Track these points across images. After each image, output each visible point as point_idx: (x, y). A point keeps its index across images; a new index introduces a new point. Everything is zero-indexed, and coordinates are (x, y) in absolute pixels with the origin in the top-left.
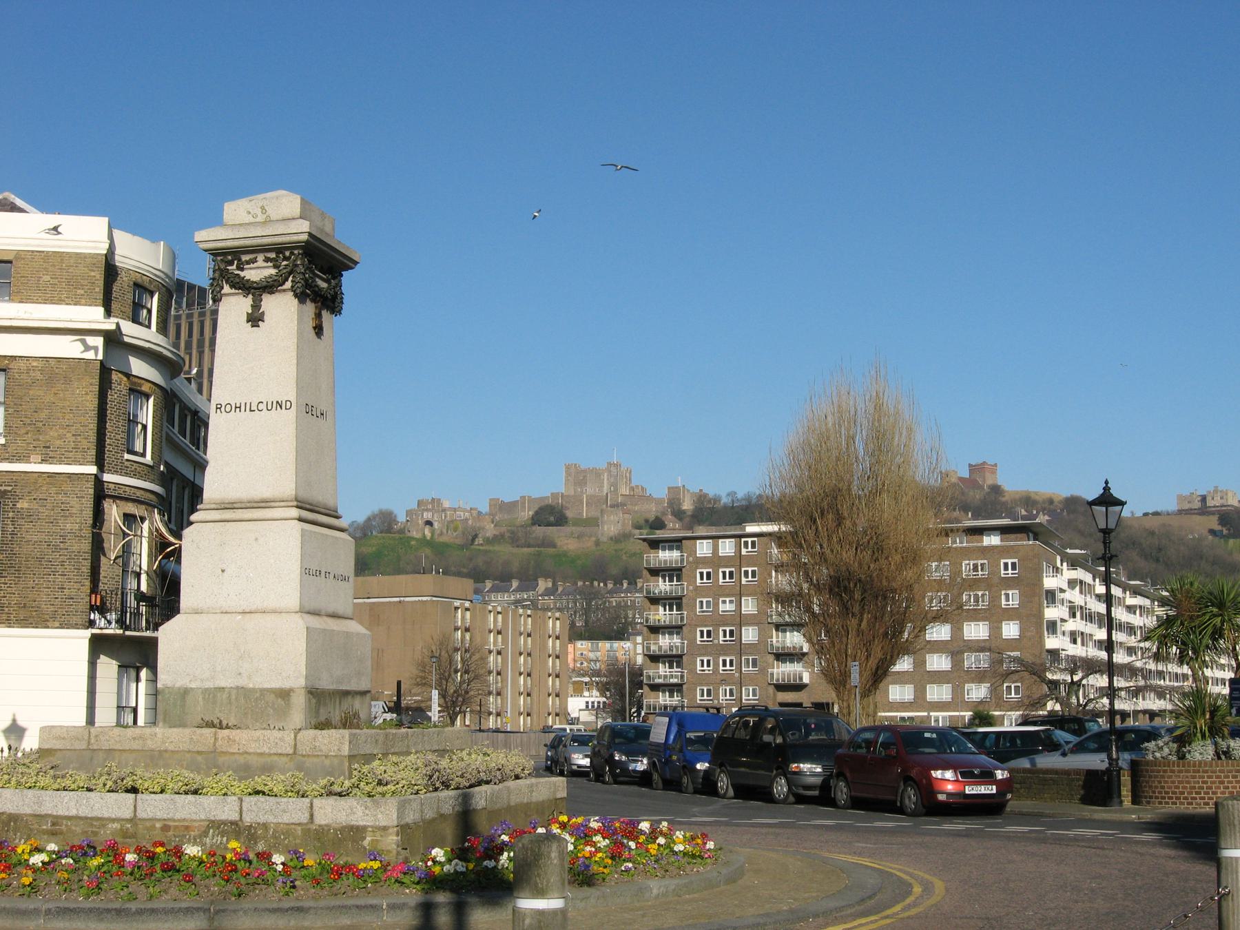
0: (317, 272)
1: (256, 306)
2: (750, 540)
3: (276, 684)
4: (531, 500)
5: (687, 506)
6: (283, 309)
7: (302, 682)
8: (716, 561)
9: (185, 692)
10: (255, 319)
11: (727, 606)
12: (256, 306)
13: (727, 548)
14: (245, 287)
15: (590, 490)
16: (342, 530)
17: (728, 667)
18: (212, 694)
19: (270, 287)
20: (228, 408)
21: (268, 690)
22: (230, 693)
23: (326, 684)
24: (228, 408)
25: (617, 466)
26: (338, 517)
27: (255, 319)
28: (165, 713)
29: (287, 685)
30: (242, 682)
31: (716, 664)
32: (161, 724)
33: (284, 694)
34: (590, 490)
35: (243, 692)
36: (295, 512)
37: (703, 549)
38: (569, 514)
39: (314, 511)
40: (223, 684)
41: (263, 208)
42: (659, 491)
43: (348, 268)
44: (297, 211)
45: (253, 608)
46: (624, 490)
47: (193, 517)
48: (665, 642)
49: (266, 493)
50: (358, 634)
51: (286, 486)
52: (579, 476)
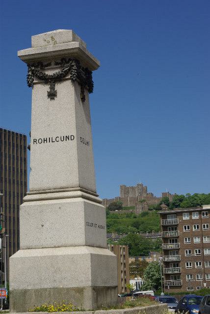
0: (79, 70)
1: (52, 88)
2: (205, 212)
3: (75, 285)
4: (107, 201)
5: (171, 200)
6: (67, 90)
7: (90, 284)
8: (192, 222)
9: (25, 292)
10: (52, 95)
11: (197, 240)
12: (52, 88)
13: (195, 217)
14: (45, 80)
15: (131, 195)
16: (99, 202)
17: (189, 266)
18: (40, 293)
19: (59, 79)
20: (40, 141)
21: (73, 289)
22: (50, 291)
23: (100, 284)
24: (40, 141)
25: (142, 185)
26: (97, 196)
27: (52, 95)
28: (14, 304)
29: (81, 285)
30: (56, 285)
31: (194, 265)
32: (12, 310)
33: (80, 291)
34: (131, 195)
35: (58, 291)
36: (79, 193)
37: (186, 218)
38: (123, 206)
39: (88, 193)
40: (46, 286)
41: (52, 38)
42: (158, 195)
43: (95, 69)
44: (71, 38)
45: (60, 245)
46: (145, 195)
47: (25, 198)
48: (172, 258)
49: (64, 185)
50: (112, 256)
51: (74, 180)
52: (125, 190)
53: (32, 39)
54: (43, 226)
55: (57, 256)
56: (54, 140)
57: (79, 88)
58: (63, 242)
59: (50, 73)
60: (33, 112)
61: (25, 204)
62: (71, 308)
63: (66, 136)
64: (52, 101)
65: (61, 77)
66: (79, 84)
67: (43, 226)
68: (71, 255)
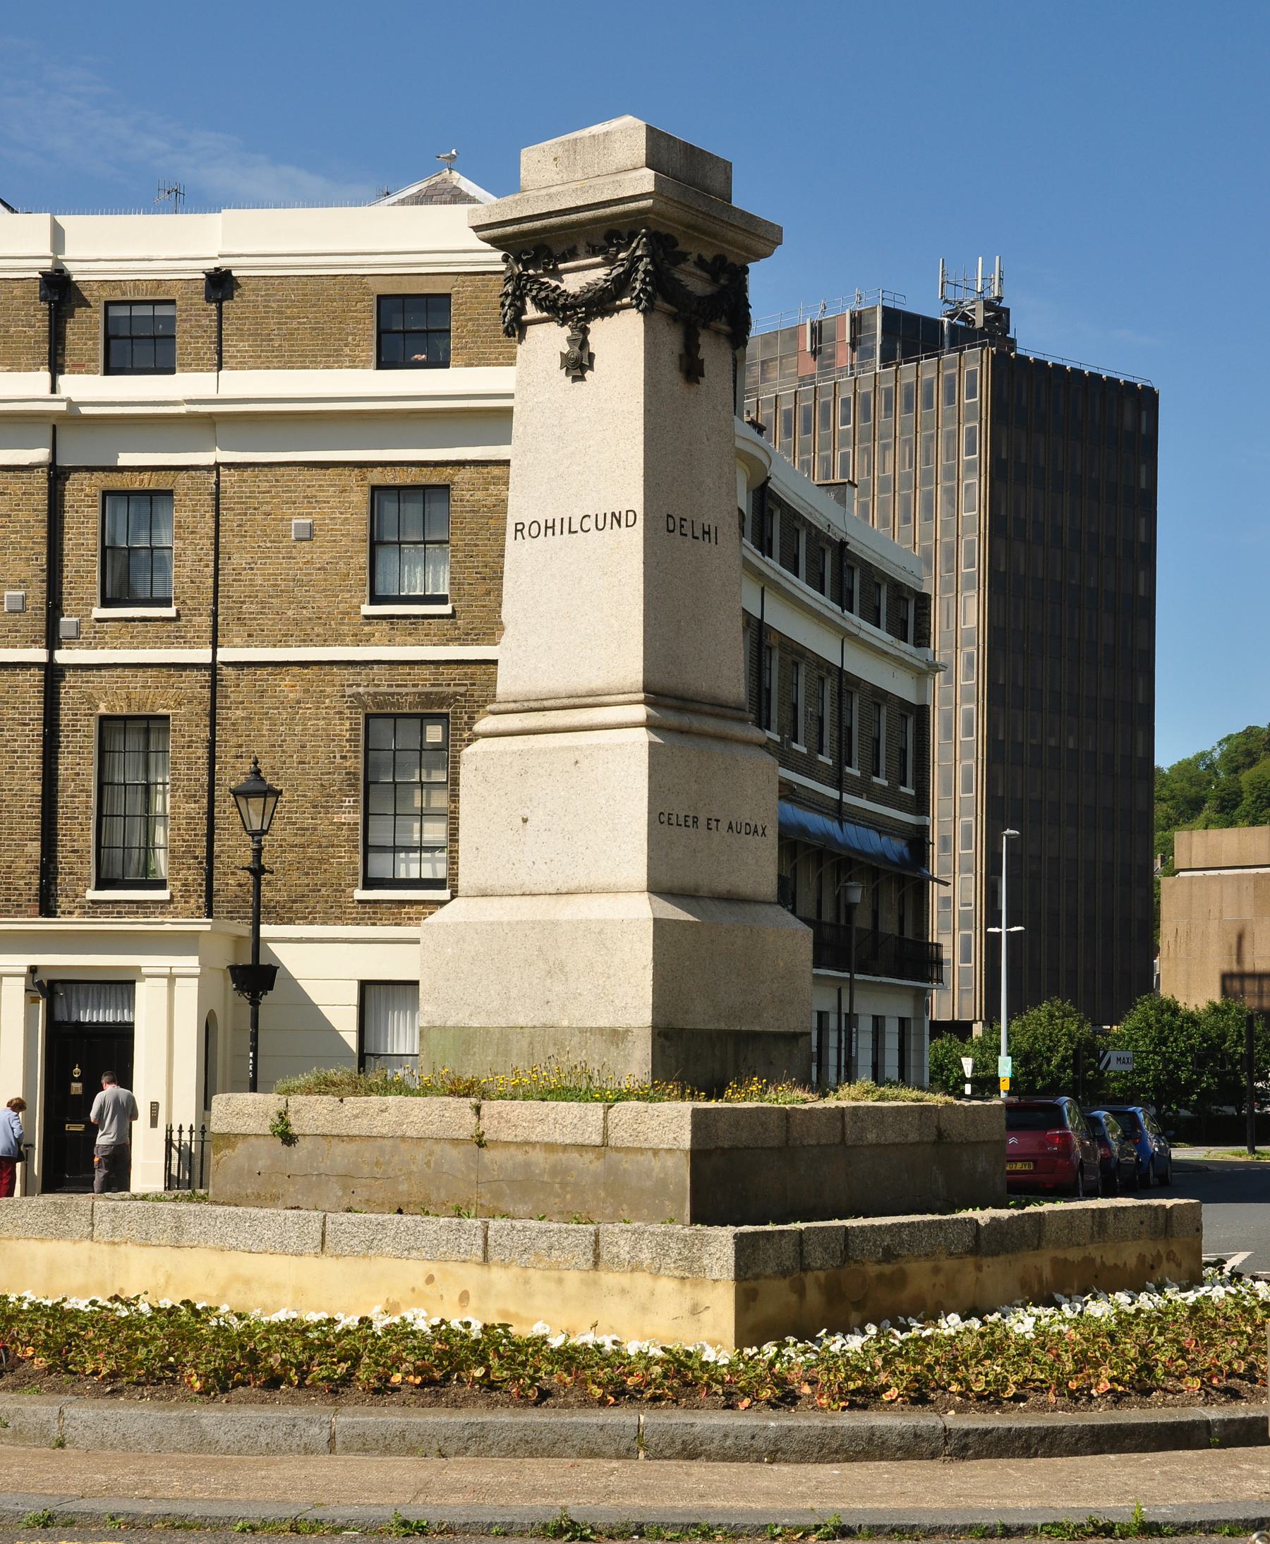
10: (578, 364)
19: (602, 303)
27: (578, 364)
29: (621, 1022)
40: (521, 1021)
45: (572, 885)
47: (485, 724)
49: (598, 683)
53: (523, 159)
54: (525, 821)
55: (555, 924)
56: (575, 527)
57: (672, 340)
58: (582, 881)
59: (573, 283)
60: (641, 438)
61: (480, 745)
62: (308, 874)
63: (613, 514)
64: (578, 384)
65: (601, 299)
66: (674, 318)
67: (525, 821)
68: (598, 921)
